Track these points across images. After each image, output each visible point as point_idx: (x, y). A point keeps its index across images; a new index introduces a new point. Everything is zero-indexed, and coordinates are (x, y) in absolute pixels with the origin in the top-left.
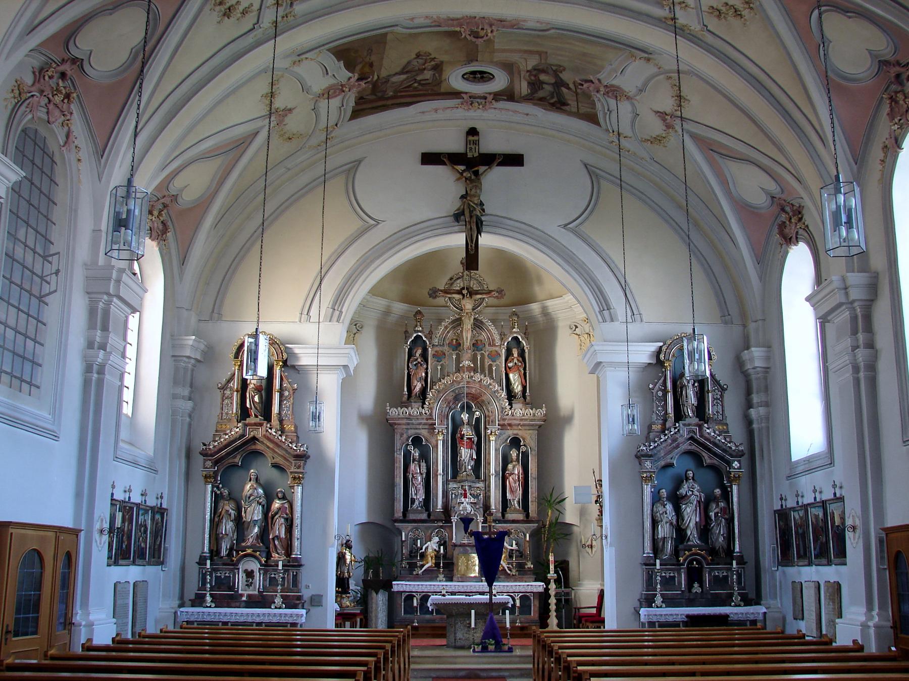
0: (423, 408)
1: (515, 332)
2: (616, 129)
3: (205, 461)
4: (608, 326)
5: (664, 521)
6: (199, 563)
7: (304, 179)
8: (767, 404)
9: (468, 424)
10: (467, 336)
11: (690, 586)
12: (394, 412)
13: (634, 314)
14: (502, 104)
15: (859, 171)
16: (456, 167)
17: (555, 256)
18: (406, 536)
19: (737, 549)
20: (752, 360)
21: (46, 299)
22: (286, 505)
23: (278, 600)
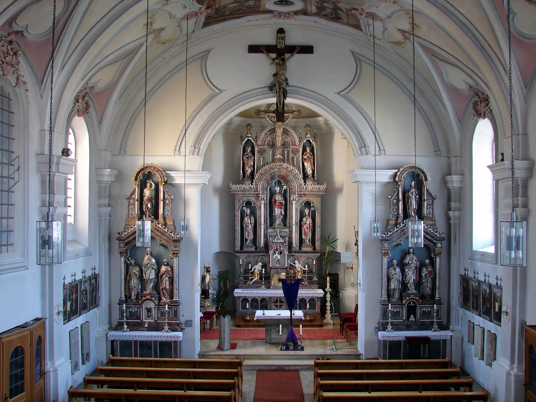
0: (252, 184)
1: (308, 137)
2: (372, 34)
3: (120, 244)
4: (364, 158)
5: (395, 279)
6: (119, 304)
7: (174, 63)
8: (460, 210)
9: (279, 193)
10: (279, 141)
11: (408, 317)
12: (234, 187)
13: (381, 150)
14: (300, 17)
15: (528, 93)
16: (270, 54)
17: (332, 113)
18: (243, 261)
19: (437, 296)
20: (452, 182)
21: (13, 189)
22: (169, 269)
23: (166, 327)
